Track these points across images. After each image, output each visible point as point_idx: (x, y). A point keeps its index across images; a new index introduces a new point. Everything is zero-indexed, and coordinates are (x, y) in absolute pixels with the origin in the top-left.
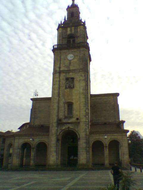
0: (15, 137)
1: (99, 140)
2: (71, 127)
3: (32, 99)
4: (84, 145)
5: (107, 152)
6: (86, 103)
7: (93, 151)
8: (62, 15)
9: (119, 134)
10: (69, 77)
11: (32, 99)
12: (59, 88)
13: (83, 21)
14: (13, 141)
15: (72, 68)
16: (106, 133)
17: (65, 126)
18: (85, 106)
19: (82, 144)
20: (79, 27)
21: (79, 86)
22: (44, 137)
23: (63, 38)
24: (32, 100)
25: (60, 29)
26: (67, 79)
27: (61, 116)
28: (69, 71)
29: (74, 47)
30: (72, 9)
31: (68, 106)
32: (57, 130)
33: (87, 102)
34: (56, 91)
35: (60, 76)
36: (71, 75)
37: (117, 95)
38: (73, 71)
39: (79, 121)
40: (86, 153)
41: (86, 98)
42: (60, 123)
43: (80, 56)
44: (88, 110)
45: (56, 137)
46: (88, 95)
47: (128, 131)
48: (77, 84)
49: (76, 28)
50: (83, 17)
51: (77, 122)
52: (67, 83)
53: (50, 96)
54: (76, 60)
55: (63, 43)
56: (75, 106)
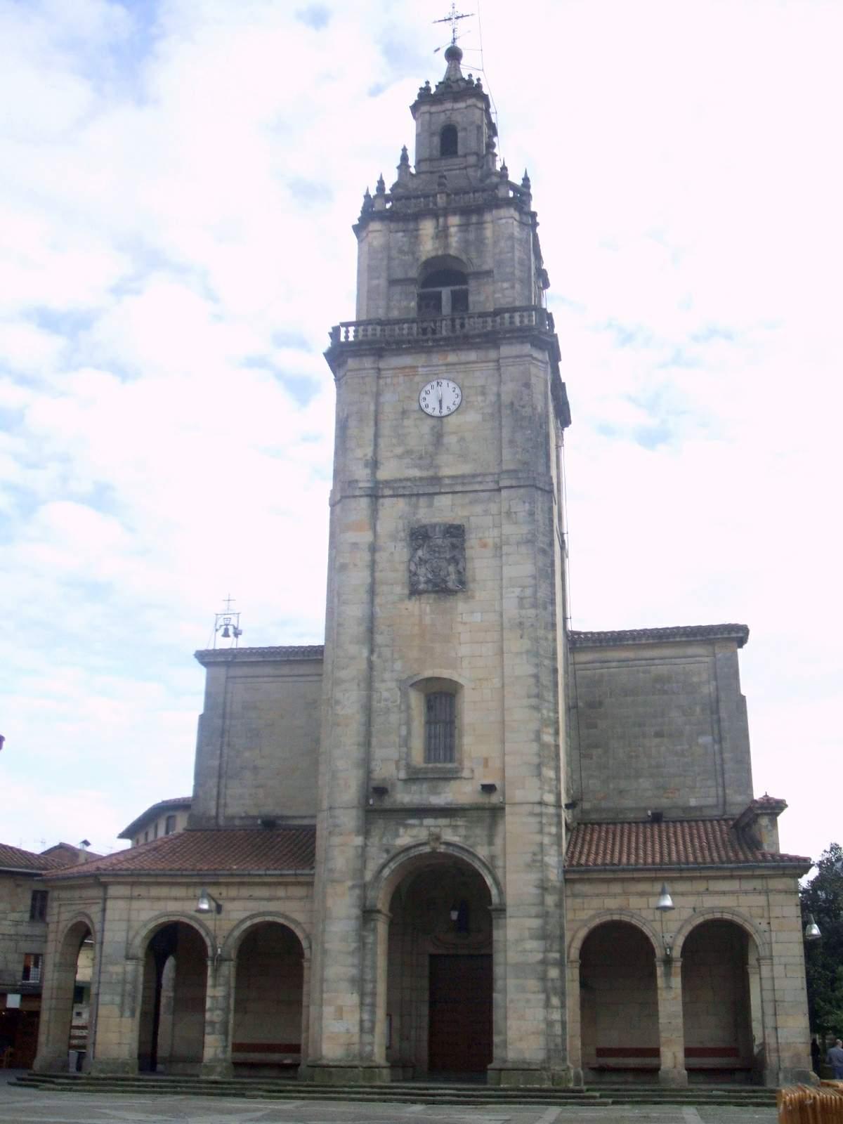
0: (105, 886)
1: (626, 918)
2: (452, 834)
3: (207, 658)
4: (533, 950)
5: (670, 995)
6: (540, 693)
7: (584, 985)
8: (385, 143)
9: (748, 885)
10: (435, 520)
11: (207, 658)
12: (372, 592)
13: (515, 177)
14: (94, 911)
15: (450, 467)
16: (664, 873)
17: (413, 826)
18: (537, 708)
19: (518, 942)
20: (488, 217)
21: (495, 573)
22: (281, 892)
23: (392, 282)
24: (205, 664)
25: (375, 226)
26: (419, 536)
27: (385, 770)
28: (432, 486)
29: (462, 341)
30: (448, 105)
31: (430, 707)
32: (363, 854)
33: (546, 679)
34: (355, 611)
35: (374, 512)
36: (444, 510)
37: (737, 635)
38: (461, 486)
39: (495, 799)
40: (542, 996)
41: (540, 655)
42: (377, 805)
43: (499, 395)
44: (557, 733)
45: (357, 892)
46: (555, 640)
47: (802, 865)
48: (480, 564)
49: (474, 219)
50: (513, 155)
51: (489, 811)
52: (422, 561)
53: (316, 638)
54: (472, 417)
55: (395, 314)
56: (473, 713)
